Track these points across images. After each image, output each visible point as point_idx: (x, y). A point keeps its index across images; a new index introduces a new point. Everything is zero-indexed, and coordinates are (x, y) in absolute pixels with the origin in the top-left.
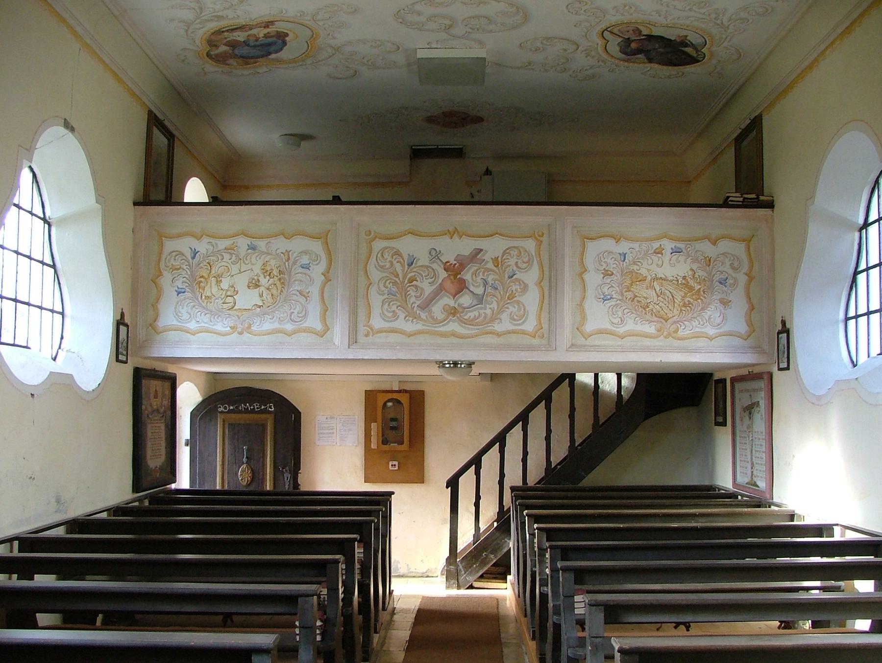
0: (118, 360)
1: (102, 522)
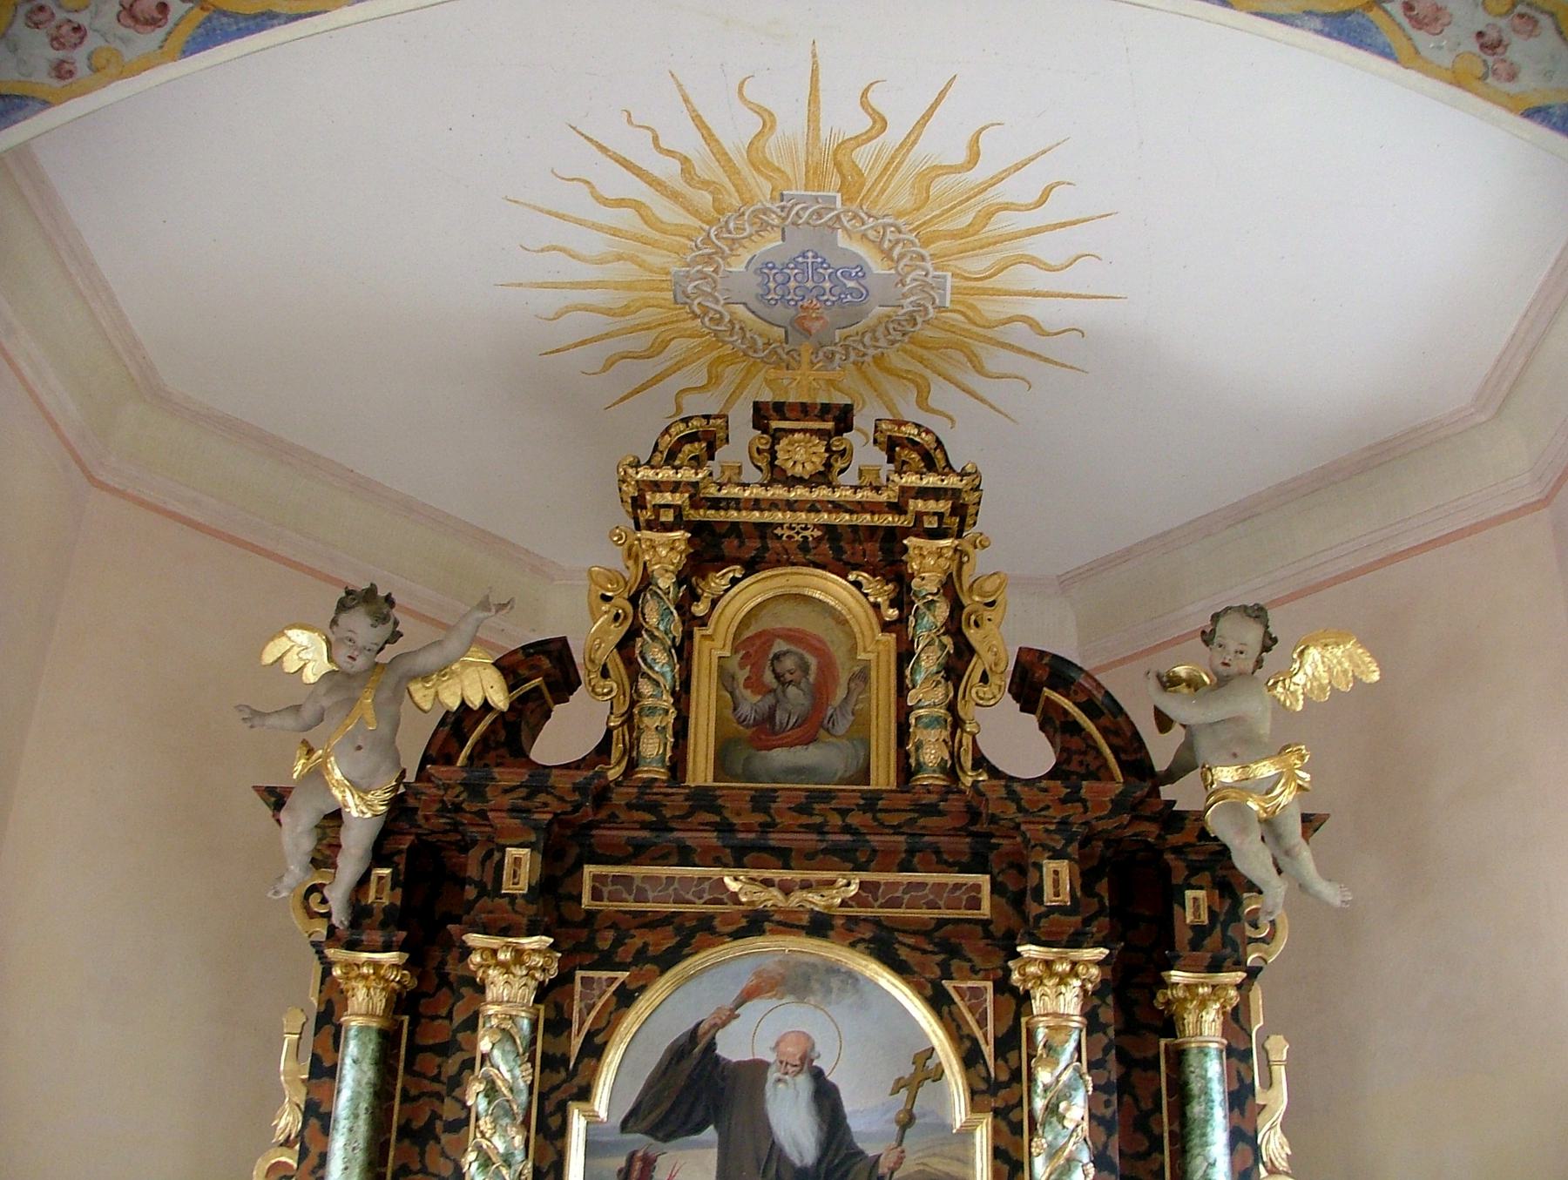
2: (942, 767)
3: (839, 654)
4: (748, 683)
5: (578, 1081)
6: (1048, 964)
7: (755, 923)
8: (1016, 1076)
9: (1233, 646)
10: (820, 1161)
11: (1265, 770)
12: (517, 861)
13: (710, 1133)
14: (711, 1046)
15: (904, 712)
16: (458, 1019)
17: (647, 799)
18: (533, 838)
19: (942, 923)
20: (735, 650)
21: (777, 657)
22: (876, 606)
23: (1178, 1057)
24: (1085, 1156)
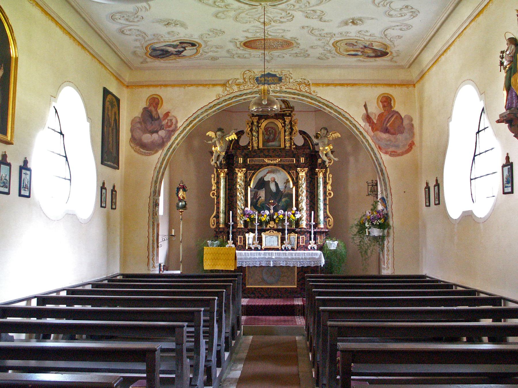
0: (101, 206)
1: (119, 281)
11: (326, 148)
13: (264, 189)
14: (264, 179)
15: (285, 139)
17: (255, 151)
19: (289, 164)
23: (317, 178)
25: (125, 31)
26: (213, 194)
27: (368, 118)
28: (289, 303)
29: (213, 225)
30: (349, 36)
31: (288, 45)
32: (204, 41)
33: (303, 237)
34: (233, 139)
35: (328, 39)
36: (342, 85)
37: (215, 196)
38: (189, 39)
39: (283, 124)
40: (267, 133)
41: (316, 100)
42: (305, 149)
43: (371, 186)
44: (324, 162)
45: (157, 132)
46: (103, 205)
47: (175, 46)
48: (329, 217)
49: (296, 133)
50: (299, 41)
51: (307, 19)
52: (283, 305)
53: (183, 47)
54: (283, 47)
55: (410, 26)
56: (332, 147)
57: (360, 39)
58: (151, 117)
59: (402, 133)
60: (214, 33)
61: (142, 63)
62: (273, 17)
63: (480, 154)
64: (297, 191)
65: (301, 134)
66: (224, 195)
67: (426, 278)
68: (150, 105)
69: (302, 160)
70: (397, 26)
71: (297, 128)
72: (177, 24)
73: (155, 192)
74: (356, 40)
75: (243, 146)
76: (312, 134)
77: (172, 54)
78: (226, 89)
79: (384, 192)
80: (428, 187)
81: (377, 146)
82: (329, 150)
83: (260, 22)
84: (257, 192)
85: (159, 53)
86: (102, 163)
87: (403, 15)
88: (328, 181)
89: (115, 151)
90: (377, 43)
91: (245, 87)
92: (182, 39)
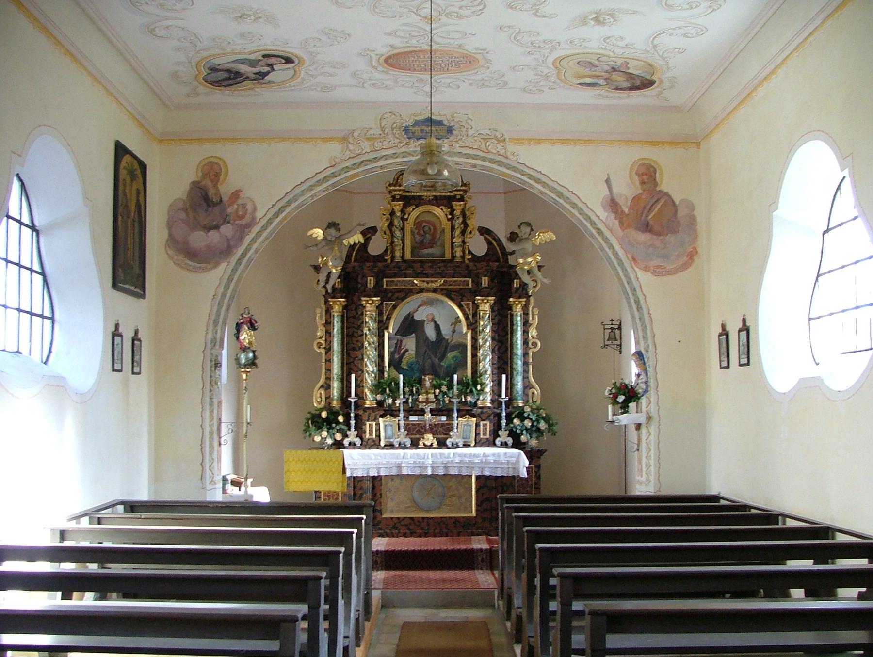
0: (114, 370)
2: (461, 257)
3: (438, 226)
4: (417, 234)
5: (386, 325)
6: (483, 300)
7: (421, 290)
8: (476, 322)
9: (523, 232)
10: (436, 340)
11: (530, 260)
12: (370, 280)
13: (414, 335)
14: (413, 317)
15: (452, 243)
16: (359, 313)
17: (397, 265)
18: (373, 275)
19: (461, 289)
20: (414, 226)
21: (424, 227)
22: (446, 214)
23: (512, 315)
24: (490, 339)
25: (157, 29)
26: (319, 345)
27: (613, 205)
28: (463, 547)
29: (319, 403)
30: (586, 47)
31: (468, 62)
32: (311, 53)
33: (486, 424)
34: (357, 242)
35: (546, 52)
36: (564, 141)
37: (324, 348)
38: (281, 49)
39: (450, 214)
40: (419, 231)
41: (515, 169)
42: (489, 260)
43: (610, 330)
44: (524, 286)
45: (217, 227)
46: (117, 367)
47: (252, 63)
48: (533, 387)
49: (473, 232)
50: (489, 56)
51: (510, 10)
52: (453, 551)
53: (268, 65)
54: (459, 67)
55: (704, 29)
56: (540, 258)
57: (607, 53)
58: (206, 199)
59: (675, 232)
60: (331, 37)
61: (188, 96)
62: (447, 7)
63: (830, 272)
64: (475, 339)
65: (481, 234)
66: (340, 347)
67: (750, 511)
68: (204, 176)
69: (485, 281)
70: (680, 28)
71: (474, 223)
72: (260, 18)
73: (214, 341)
74: (599, 56)
75: (374, 256)
76: (503, 236)
77: (247, 78)
78: (348, 148)
79: (642, 343)
80: (725, 333)
81: (630, 256)
82: (533, 264)
83: (419, 15)
84: (401, 341)
85: (223, 75)
86: (115, 286)
87: (694, 5)
88: (530, 321)
89: (137, 263)
90: (636, 61)
91: (384, 143)
92: (268, 48)
